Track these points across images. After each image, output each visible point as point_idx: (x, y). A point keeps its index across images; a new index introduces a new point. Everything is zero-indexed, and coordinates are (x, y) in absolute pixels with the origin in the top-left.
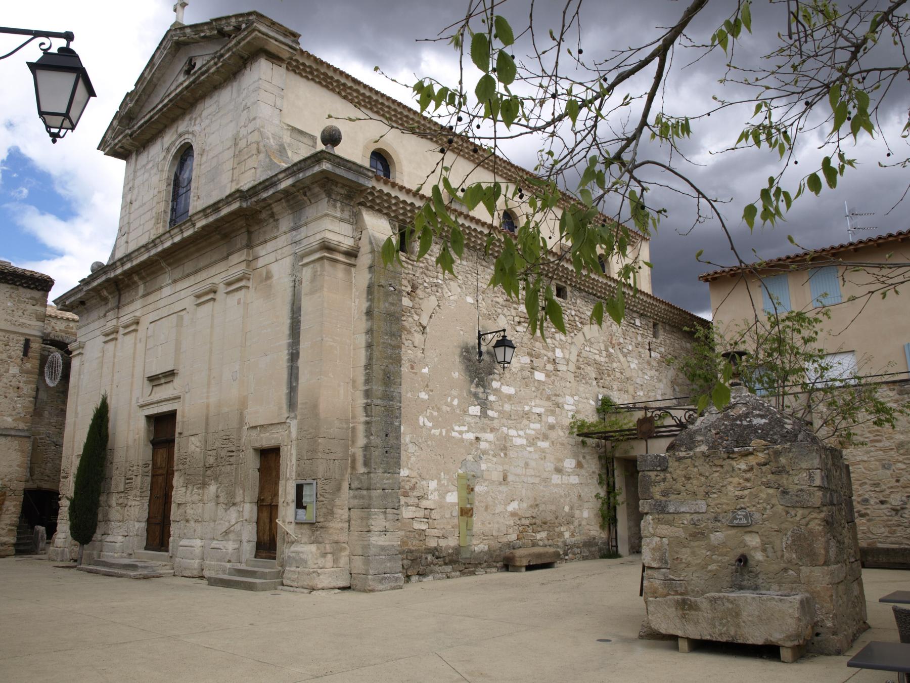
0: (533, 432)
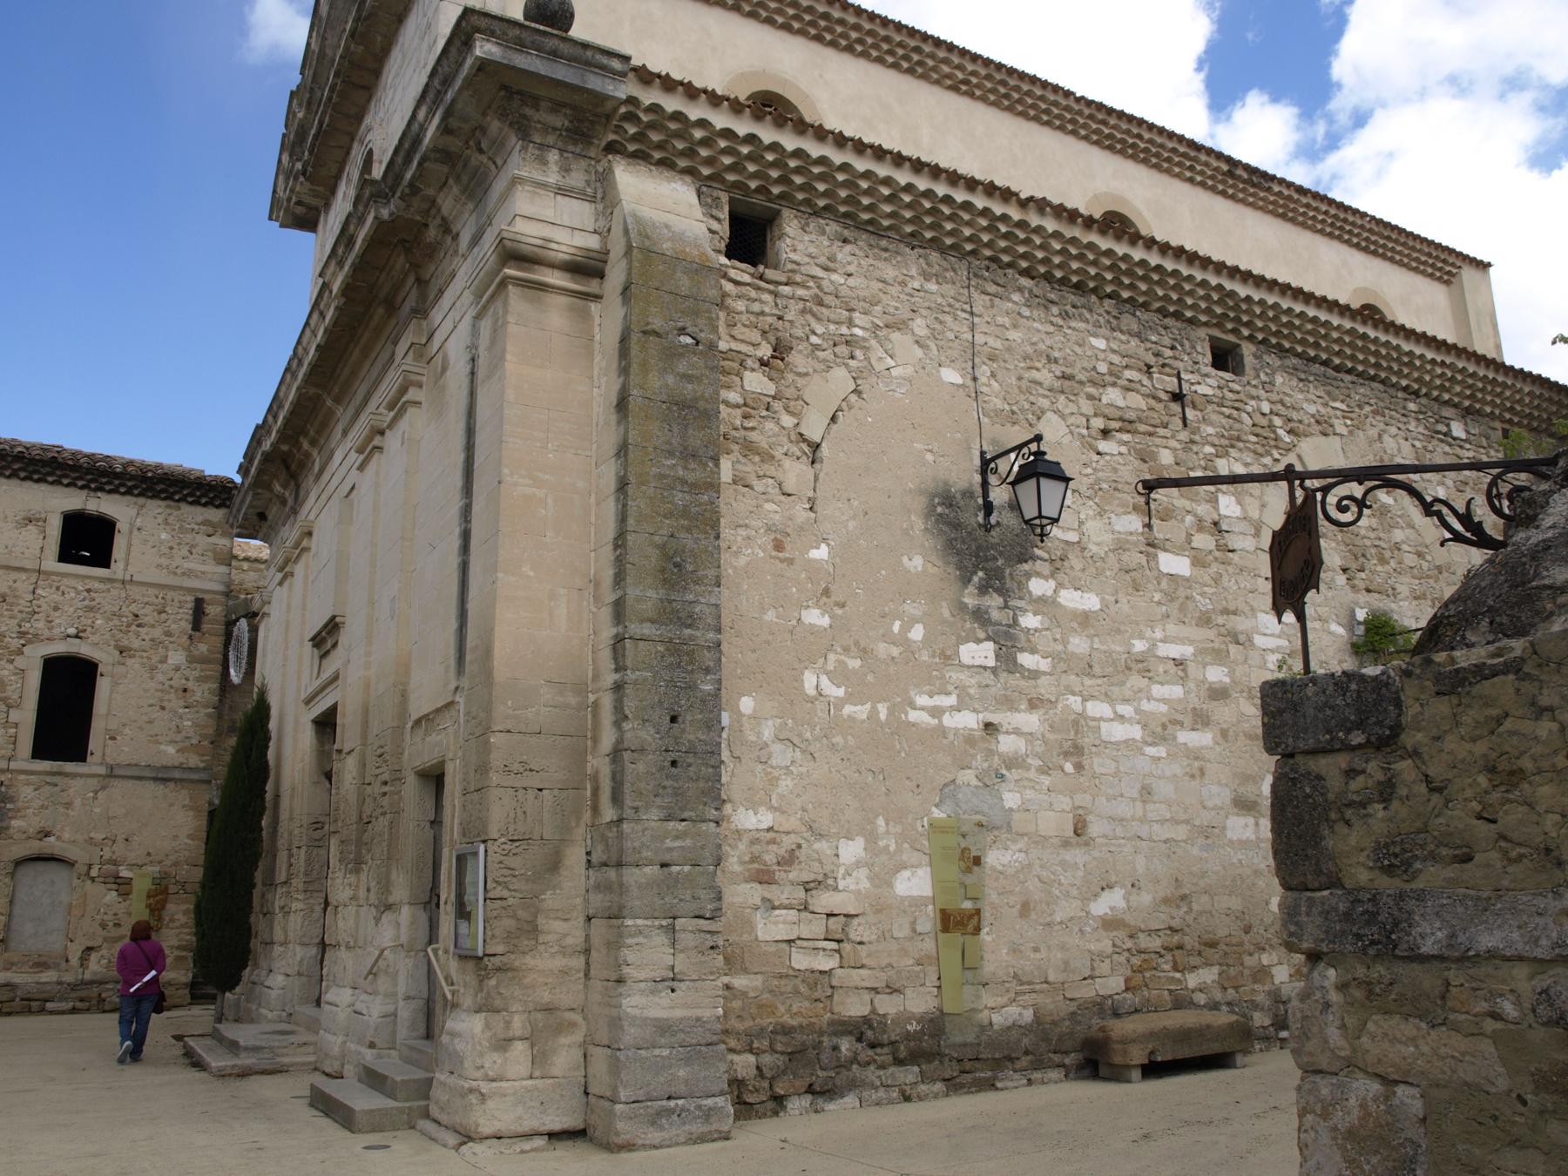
0: (1163, 708)
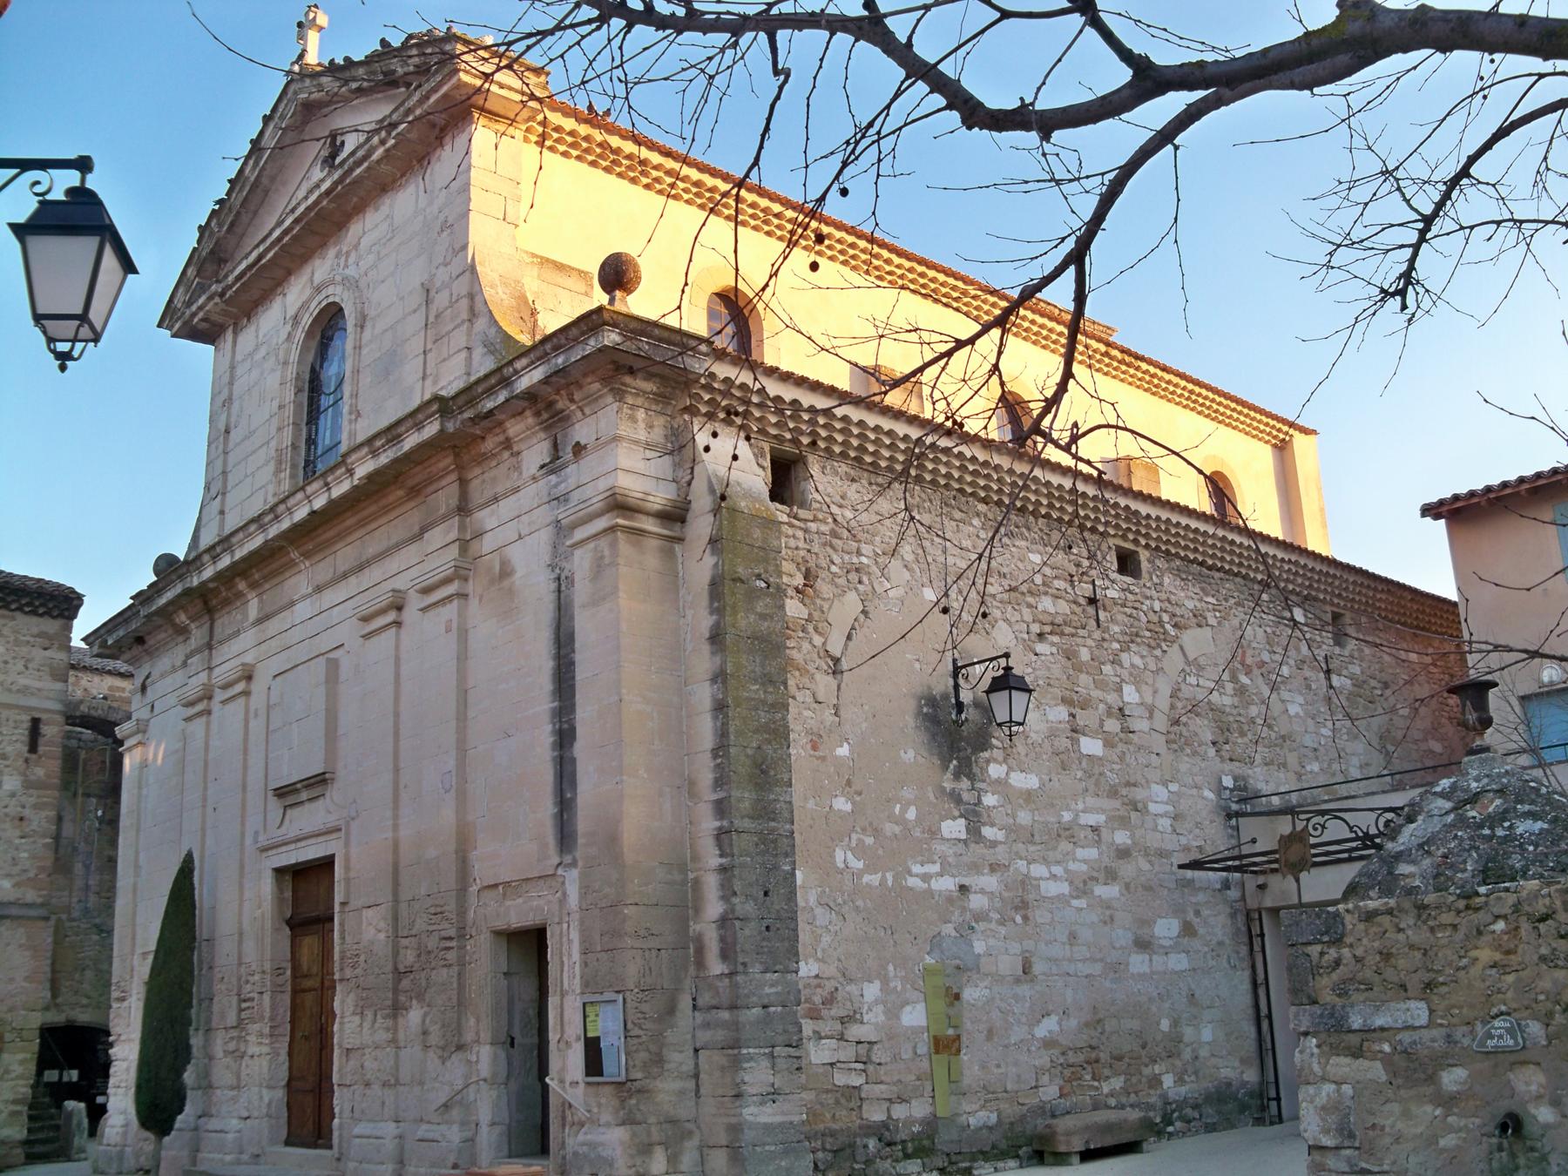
0: (1084, 867)
